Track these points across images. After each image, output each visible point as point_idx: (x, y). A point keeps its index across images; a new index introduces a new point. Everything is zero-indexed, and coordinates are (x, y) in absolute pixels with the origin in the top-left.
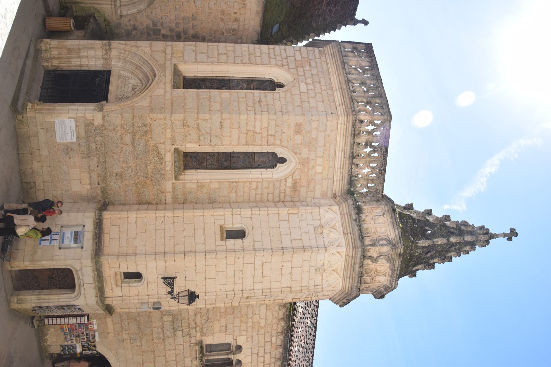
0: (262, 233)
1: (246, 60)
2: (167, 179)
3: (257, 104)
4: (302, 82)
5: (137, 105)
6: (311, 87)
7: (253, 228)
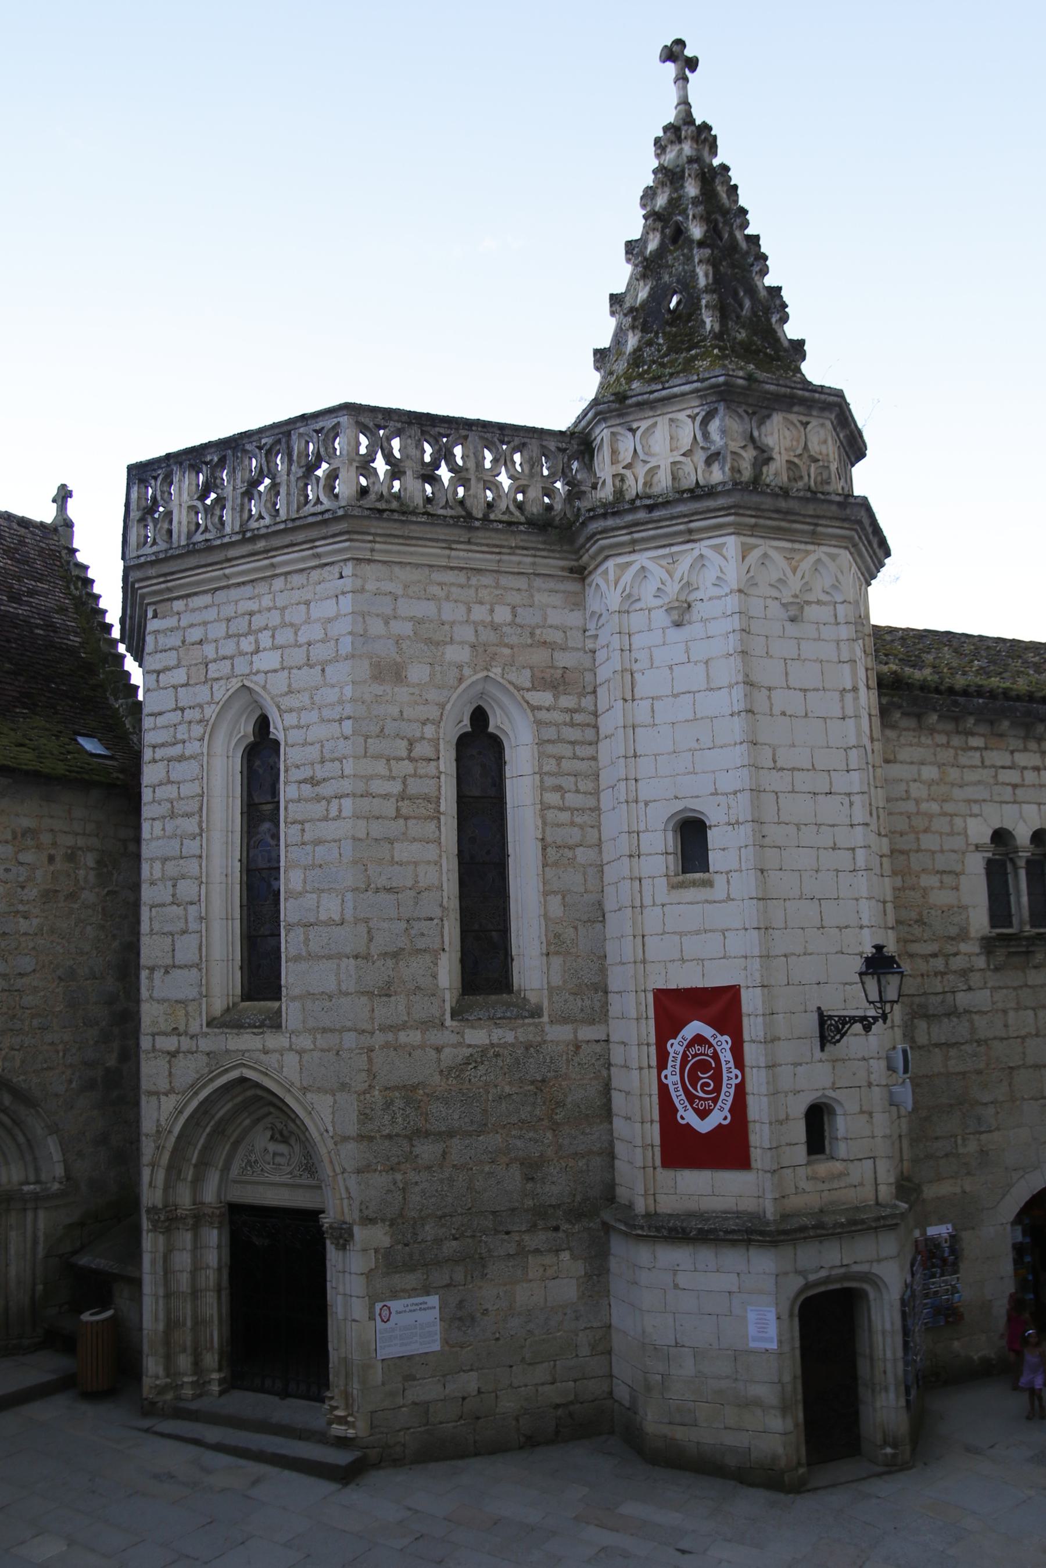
0: (689, 773)
1: (190, 825)
2: (539, 1039)
3: (318, 789)
4: (252, 663)
5: (330, 1129)
6: (265, 640)
7: (676, 798)
